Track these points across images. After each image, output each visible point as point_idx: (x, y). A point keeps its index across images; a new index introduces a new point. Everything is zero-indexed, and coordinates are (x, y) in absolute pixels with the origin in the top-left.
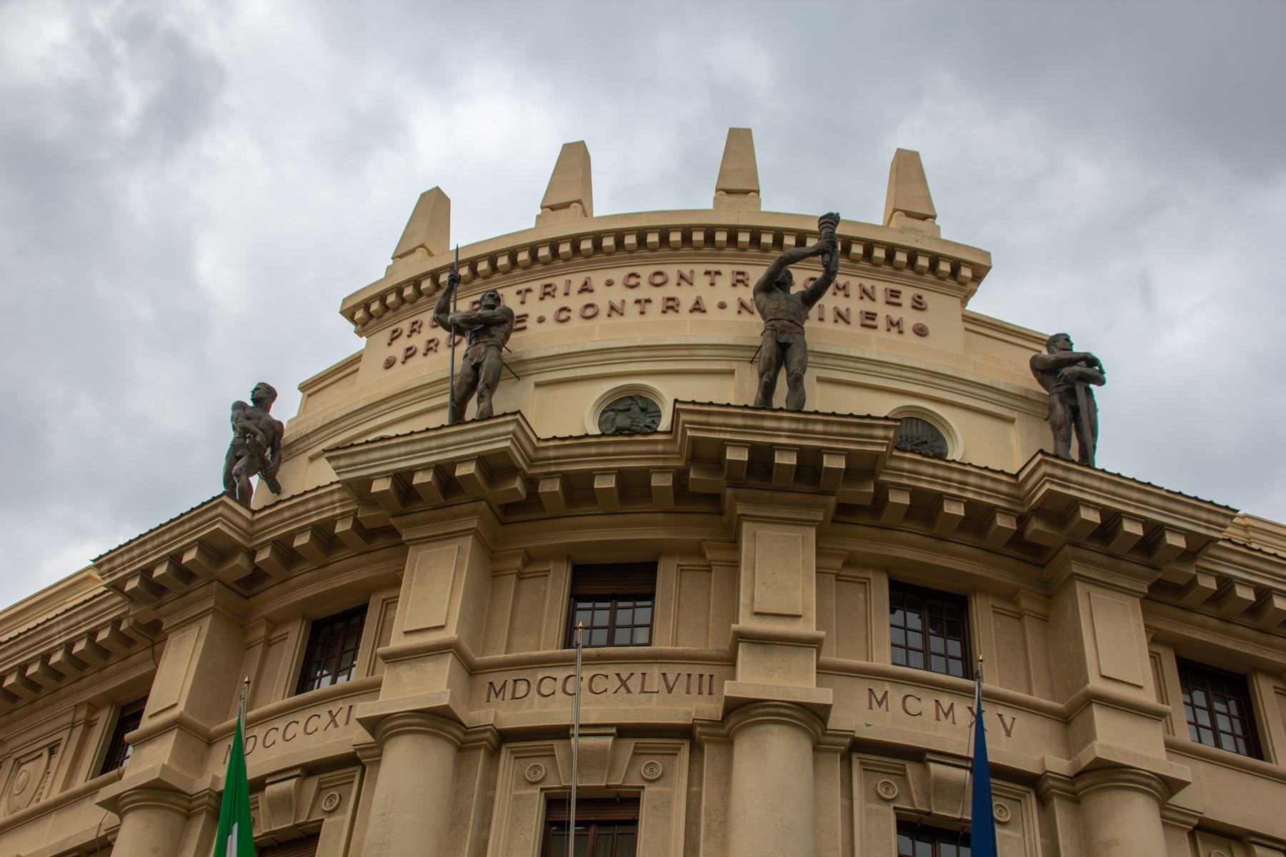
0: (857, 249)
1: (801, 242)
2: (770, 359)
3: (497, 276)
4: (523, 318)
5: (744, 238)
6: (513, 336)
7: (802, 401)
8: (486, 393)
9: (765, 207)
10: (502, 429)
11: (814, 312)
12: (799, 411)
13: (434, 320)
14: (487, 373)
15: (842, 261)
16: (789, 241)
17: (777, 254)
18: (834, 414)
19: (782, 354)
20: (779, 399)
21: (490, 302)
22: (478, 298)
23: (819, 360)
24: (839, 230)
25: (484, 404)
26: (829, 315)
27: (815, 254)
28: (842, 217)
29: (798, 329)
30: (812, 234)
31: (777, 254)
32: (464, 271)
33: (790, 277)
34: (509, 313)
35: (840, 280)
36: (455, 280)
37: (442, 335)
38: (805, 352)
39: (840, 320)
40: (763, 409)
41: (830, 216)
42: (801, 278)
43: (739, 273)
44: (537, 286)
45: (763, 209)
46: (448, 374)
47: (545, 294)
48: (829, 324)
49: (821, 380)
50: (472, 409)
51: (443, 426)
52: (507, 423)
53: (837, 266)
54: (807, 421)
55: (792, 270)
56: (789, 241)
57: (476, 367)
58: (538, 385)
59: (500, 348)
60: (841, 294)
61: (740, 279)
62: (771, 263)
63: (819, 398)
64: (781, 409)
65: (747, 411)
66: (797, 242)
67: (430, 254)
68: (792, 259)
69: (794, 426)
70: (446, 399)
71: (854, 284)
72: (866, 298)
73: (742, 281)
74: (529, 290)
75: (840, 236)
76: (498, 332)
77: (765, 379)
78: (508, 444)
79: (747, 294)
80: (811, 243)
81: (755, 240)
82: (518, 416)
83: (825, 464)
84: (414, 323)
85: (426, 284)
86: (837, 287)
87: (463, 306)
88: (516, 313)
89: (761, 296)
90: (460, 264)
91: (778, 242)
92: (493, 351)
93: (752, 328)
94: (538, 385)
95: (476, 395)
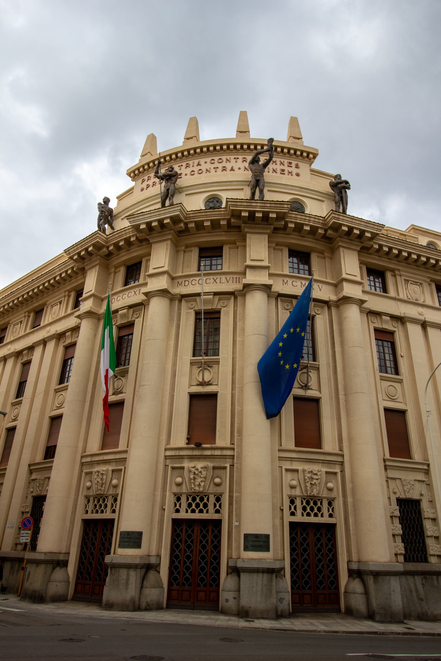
0: (279, 149)
1: (262, 148)
3: (172, 161)
4: (181, 174)
5: (245, 147)
6: (178, 180)
8: (171, 198)
9: (251, 137)
10: (177, 209)
11: (266, 170)
12: (263, 200)
13: (155, 175)
14: (171, 192)
15: (275, 153)
16: (259, 147)
17: (255, 152)
18: (273, 201)
19: (257, 183)
20: (257, 197)
21: (171, 169)
22: (167, 168)
23: (268, 185)
25: (171, 201)
26: (271, 171)
28: (275, 139)
30: (266, 145)
31: (255, 152)
32: (162, 160)
34: (176, 173)
35: (274, 159)
36: (160, 163)
37: (157, 180)
38: (264, 182)
40: (252, 200)
42: (263, 159)
43: (244, 158)
44: (184, 164)
45: (251, 137)
46: (160, 192)
47: (224, 170)
48: (271, 173)
49: (269, 191)
50: (167, 203)
51: (159, 208)
52: (178, 206)
53: (273, 155)
54: (265, 203)
55: (260, 157)
56: (259, 147)
57: (168, 190)
58: (186, 195)
59: (174, 184)
60: (274, 164)
61: (244, 160)
62: (254, 154)
63: (268, 196)
64: (257, 200)
67: (152, 155)
68: (260, 153)
69: (261, 205)
70: (160, 200)
73: (245, 161)
74: (182, 165)
75: (274, 145)
76: (174, 179)
77: (252, 191)
78: (179, 213)
79: (247, 165)
80: (265, 148)
81: (249, 148)
82: (181, 205)
84: (149, 177)
85: (151, 165)
86: (273, 162)
87: (163, 171)
88: (179, 173)
89: (251, 165)
90: (161, 158)
92: (172, 185)
93: (248, 175)
94: (186, 195)
95: (168, 199)
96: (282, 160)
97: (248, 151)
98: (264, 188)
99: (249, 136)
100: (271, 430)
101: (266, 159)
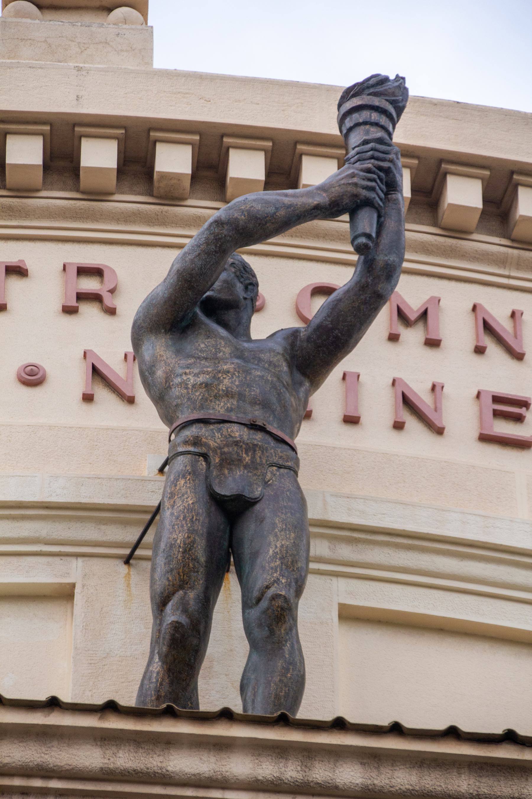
0: (464, 194)
1: (283, 171)
2: (188, 549)
5: (99, 156)
7: (294, 686)
9: (166, 56)
11: (327, 397)
12: (284, 721)
15: (416, 232)
16: (246, 166)
17: (206, 210)
18: (396, 729)
19: (227, 534)
20: (220, 680)
23: (345, 552)
24: (407, 132)
26: (378, 407)
27: (330, 209)
28: (414, 89)
29: (277, 452)
30: (318, 143)
31: (206, 210)
33: (251, 283)
35: (410, 292)
38: (300, 526)
39: (412, 423)
40: (170, 713)
41: (376, 85)
42: (287, 287)
43: (83, 271)
45: (161, 61)
48: (376, 434)
49: (350, 616)
53: (398, 246)
54: (309, 752)
55: (255, 263)
56: (246, 166)
60: (412, 337)
61: (88, 292)
62: (191, 237)
63: (349, 676)
64: (226, 715)
65: (114, 723)
66: (269, 173)
68: (255, 229)
69: (267, 769)
71: (456, 306)
72: (493, 349)
73: (95, 298)
75: (409, 152)
77: (172, 615)
79: (111, 339)
80: (317, 173)
81: (136, 165)
83: (10, 159)
86: (401, 315)
89: (158, 347)
91: (210, 171)
93: (130, 452)
96: (499, 306)
97: (129, 201)
98: (299, 592)
99: (146, 51)
100: (480, 218)
101: (321, 290)
